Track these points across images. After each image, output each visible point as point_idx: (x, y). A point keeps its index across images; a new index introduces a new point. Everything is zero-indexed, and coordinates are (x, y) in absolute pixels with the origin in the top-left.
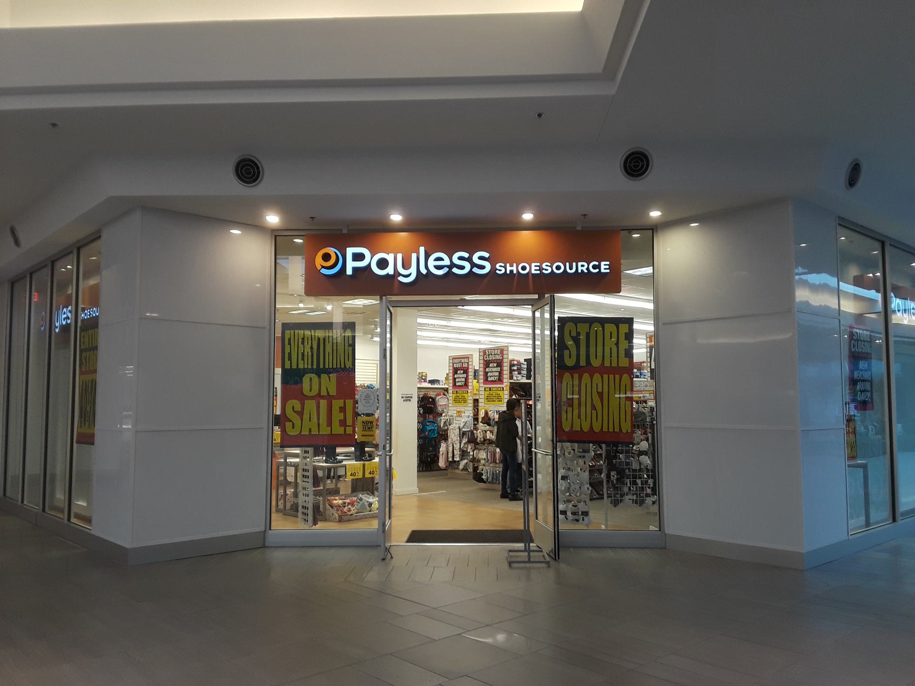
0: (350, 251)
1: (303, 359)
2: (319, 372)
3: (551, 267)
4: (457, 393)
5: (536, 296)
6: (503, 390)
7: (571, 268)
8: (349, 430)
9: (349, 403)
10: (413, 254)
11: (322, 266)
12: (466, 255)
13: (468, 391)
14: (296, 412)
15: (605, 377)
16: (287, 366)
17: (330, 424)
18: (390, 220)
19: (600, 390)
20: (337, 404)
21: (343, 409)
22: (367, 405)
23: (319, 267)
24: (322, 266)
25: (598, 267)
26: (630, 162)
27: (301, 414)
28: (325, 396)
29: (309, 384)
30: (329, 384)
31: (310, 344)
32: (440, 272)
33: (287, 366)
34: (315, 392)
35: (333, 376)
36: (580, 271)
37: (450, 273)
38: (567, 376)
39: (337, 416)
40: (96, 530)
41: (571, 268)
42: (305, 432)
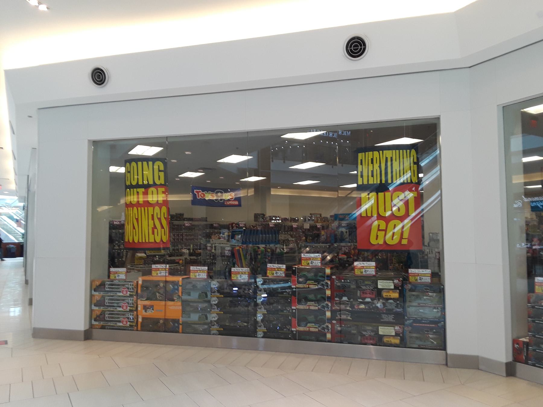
1: (373, 176)
10: (111, 171)
15: (139, 209)
26: (351, 47)
28: (365, 216)
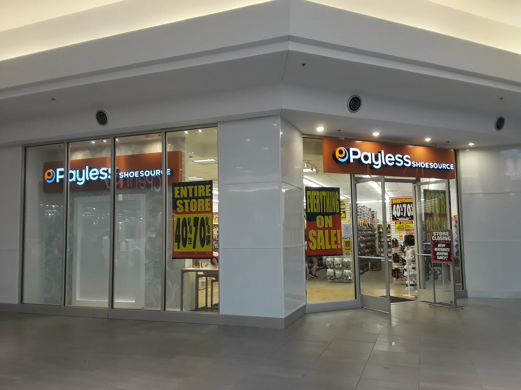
0: (352, 150)
2: (324, 214)
3: (144, 173)
4: (400, 223)
5: (414, 179)
6: (412, 223)
7: (153, 173)
8: (339, 247)
9: (339, 231)
11: (339, 156)
12: (401, 156)
13: (412, 222)
14: (314, 237)
16: (309, 211)
17: (330, 243)
18: (373, 136)
19: (440, 225)
20: (333, 232)
21: (336, 235)
22: (347, 233)
23: (338, 157)
24: (339, 156)
25: (449, 166)
27: (316, 238)
29: (320, 221)
30: (329, 221)
31: (319, 198)
32: (391, 164)
33: (309, 211)
34: (322, 226)
35: (331, 217)
36: (157, 175)
37: (395, 165)
38: (428, 218)
39: (333, 239)
40: (223, 311)
41: (153, 173)
42: (319, 248)
